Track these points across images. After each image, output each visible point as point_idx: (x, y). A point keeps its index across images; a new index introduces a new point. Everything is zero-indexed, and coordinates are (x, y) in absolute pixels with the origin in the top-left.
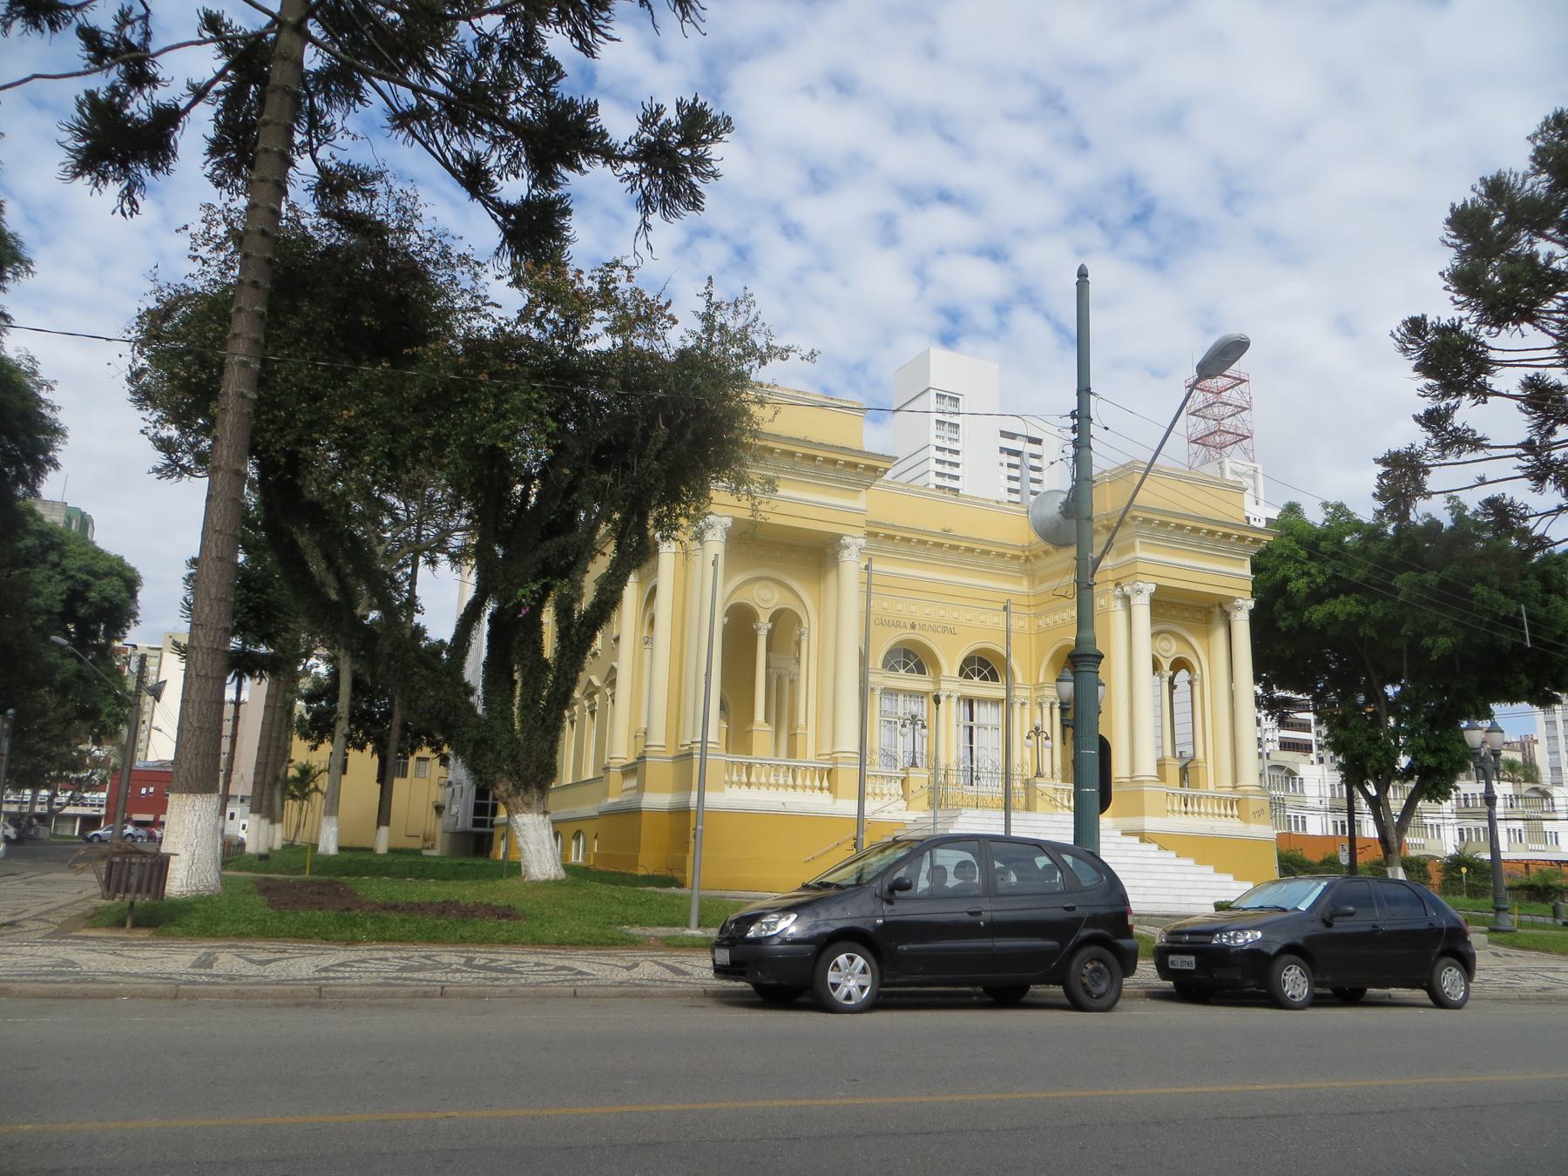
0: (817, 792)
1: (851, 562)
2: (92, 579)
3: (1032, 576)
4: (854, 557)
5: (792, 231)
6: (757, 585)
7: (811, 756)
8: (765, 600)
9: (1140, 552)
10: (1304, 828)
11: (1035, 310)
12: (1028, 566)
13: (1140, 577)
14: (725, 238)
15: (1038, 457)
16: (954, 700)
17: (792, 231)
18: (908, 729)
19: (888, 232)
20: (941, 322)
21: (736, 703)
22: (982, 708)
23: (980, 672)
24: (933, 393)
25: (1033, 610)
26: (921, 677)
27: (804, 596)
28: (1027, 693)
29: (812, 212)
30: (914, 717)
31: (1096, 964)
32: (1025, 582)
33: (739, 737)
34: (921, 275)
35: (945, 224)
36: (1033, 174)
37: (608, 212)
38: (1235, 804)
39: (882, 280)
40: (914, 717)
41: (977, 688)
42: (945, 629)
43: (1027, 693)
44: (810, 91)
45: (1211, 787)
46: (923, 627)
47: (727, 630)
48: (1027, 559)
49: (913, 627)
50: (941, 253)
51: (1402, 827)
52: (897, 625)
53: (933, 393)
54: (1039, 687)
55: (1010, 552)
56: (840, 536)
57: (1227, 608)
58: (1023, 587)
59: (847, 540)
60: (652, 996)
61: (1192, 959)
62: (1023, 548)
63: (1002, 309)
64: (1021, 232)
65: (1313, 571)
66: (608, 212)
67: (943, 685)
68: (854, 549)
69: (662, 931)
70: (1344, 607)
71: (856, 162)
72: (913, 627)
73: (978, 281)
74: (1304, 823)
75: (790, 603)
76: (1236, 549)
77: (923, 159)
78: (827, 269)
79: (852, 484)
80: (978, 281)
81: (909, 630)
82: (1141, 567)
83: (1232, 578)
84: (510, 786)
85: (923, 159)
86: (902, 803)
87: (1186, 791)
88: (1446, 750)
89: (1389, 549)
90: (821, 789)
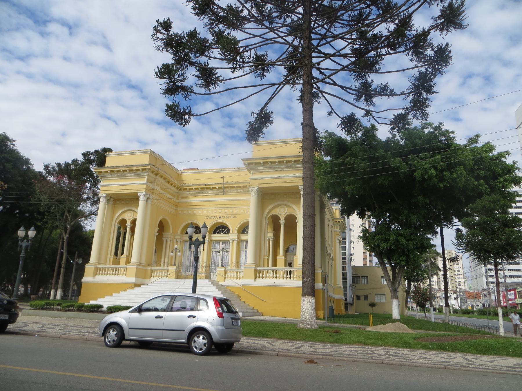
5: (506, 64)
14: (478, 75)
17: (506, 64)
33: (117, 262)
52: (214, 218)
56: (137, 193)
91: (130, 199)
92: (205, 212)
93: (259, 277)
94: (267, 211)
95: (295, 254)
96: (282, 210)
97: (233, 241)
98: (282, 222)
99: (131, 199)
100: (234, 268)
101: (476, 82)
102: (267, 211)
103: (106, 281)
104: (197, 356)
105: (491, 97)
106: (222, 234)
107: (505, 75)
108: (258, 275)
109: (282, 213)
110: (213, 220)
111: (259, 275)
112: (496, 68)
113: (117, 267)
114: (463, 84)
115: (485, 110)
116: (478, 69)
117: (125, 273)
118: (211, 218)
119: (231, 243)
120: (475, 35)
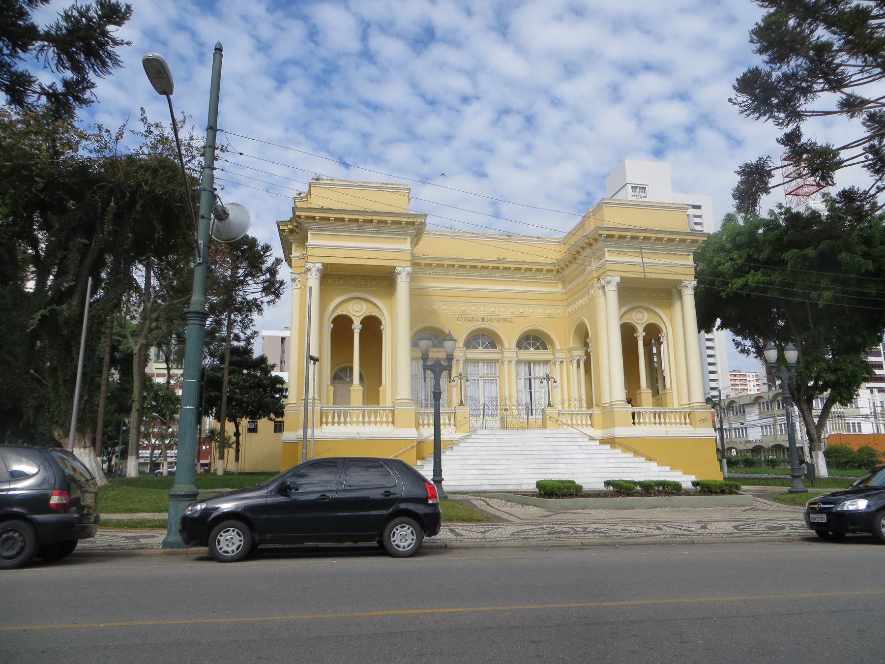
0: (373, 425)
1: (402, 285)
2: (120, 339)
3: (564, 282)
4: (404, 278)
5: (556, 103)
6: (352, 303)
7: (676, 406)
8: (640, 320)
9: (608, 257)
10: (860, 430)
11: (711, 127)
12: (560, 275)
13: (608, 273)
14: (518, 112)
15: (699, 217)
16: (514, 363)
17: (556, 103)
18: (545, 382)
19: (615, 94)
20: (653, 143)
21: (341, 374)
22: (537, 367)
23: (534, 345)
24: (629, 186)
25: (565, 303)
26: (494, 350)
27: (381, 308)
28: (564, 355)
29: (568, 90)
30: (548, 376)
31: (20, 544)
32: (560, 285)
33: (341, 398)
34: (637, 116)
35: (650, 83)
36: (702, 44)
37: (451, 108)
38: (688, 415)
39: (615, 123)
40: (460, 375)
41: (531, 354)
42: (505, 320)
43: (564, 355)
44: (559, 18)
45: (676, 406)
46: (490, 320)
47: (334, 332)
48: (558, 271)
49: (483, 320)
50: (648, 101)
51: (821, 425)
52: (472, 320)
53: (629, 186)
54: (570, 351)
55: (545, 268)
56: (394, 267)
57: (679, 288)
58: (559, 288)
59: (398, 269)
60: (499, 547)
61: (824, 516)
62: (554, 264)
63: (690, 130)
64: (698, 81)
65: (735, 256)
66: (451, 108)
67: (505, 354)
68: (404, 274)
69: (125, 517)
70: (753, 278)
71: (590, 56)
72: (483, 320)
73: (673, 115)
74: (859, 427)
75: (373, 312)
76: (657, 247)
77: (630, 46)
78: (581, 121)
79: (400, 235)
80: (673, 115)
81: (481, 323)
82: (608, 266)
83: (682, 268)
84: (61, 433)
85: (630, 46)
86: (453, 428)
87: (658, 410)
88: (840, 369)
89: (781, 235)
90: (686, 424)
91: (369, 277)
92: (454, 308)
93: (327, 423)
94: (332, 306)
95: (380, 384)
96: (639, 316)
97: (510, 361)
98: (357, 327)
99: (381, 279)
100: (584, 409)
101: (513, 122)
102: (332, 306)
103: (355, 435)
104: (228, 564)
105: (528, 148)
106: (481, 348)
107: (553, 118)
108: (324, 420)
109: (357, 311)
110: (474, 323)
111: (327, 419)
112: (542, 107)
113: (375, 408)
114: (495, 122)
115: (518, 166)
116: (519, 103)
117: (589, 422)
118: (466, 320)
119: (506, 366)
120: (520, 50)
